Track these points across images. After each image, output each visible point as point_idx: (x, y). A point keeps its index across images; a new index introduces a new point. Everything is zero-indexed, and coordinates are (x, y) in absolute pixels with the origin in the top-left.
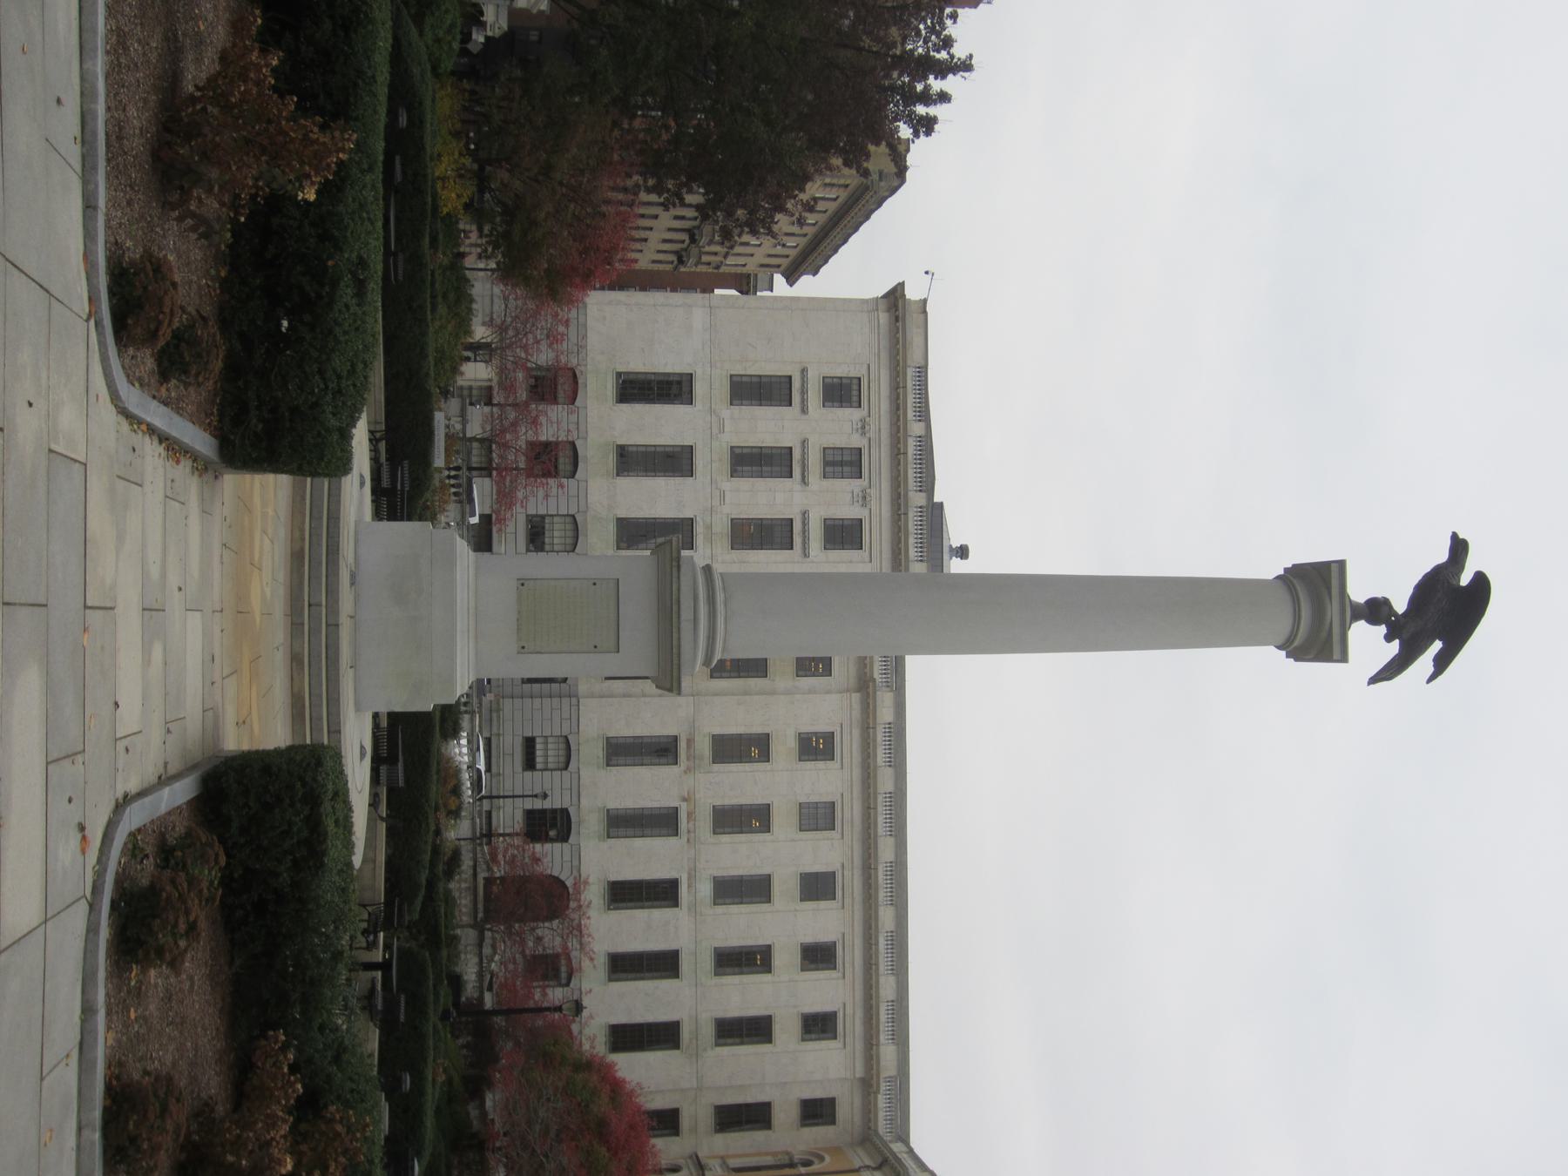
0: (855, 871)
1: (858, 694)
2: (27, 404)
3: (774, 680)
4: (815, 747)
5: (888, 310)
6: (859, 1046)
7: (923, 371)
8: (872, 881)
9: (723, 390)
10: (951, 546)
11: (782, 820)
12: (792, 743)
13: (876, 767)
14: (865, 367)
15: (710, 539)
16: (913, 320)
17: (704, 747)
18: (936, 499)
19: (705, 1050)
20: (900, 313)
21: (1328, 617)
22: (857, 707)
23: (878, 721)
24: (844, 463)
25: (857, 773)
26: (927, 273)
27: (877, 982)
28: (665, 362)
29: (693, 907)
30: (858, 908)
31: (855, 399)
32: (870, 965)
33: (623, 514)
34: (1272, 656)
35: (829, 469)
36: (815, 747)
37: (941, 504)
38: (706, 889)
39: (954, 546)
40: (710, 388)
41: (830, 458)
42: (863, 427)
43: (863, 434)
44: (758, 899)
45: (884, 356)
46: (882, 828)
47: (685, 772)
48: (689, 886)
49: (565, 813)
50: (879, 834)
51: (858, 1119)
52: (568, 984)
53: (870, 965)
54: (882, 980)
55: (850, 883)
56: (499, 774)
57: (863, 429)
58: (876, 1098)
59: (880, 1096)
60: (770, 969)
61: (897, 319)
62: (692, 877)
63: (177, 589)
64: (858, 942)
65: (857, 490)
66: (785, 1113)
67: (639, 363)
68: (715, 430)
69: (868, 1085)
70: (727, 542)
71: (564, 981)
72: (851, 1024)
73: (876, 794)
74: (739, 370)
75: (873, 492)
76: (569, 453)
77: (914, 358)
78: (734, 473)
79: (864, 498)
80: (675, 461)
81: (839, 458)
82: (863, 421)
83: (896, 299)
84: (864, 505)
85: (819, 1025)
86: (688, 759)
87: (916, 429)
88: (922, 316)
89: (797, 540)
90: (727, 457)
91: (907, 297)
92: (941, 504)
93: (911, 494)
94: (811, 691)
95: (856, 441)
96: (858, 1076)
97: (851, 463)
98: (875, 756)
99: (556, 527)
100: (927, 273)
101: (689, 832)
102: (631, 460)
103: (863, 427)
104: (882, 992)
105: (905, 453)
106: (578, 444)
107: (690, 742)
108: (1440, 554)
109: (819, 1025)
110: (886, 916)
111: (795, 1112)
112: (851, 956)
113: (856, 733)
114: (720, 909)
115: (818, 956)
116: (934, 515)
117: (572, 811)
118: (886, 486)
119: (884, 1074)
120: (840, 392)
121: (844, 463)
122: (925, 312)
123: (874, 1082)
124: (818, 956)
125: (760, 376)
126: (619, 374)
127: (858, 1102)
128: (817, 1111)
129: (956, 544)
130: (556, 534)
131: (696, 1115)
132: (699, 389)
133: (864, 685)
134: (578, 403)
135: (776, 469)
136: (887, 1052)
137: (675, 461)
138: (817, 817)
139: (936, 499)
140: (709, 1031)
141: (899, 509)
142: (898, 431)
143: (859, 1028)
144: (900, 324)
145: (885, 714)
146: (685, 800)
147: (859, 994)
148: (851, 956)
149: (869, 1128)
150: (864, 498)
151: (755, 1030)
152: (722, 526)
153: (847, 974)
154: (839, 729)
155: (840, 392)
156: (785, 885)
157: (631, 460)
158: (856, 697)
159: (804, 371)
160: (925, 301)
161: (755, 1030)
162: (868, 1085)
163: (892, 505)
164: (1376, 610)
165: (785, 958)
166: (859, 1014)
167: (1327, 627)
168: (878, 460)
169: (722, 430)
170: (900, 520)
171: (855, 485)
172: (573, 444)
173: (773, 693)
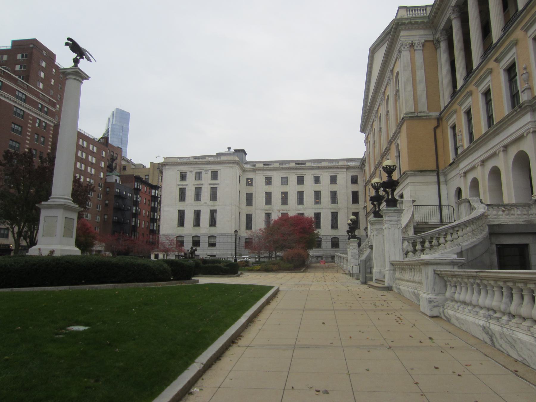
0: (297, 172)
1: (257, 172)
2: (368, 352)
3: (253, 191)
4: (268, 181)
5: (166, 166)
6: (338, 170)
7: (180, 158)
8: (299, 168)
9: (182, 203)
10: (228, 151)
11: (285, 189)
12: (267, 187)
13: (273, 167)
14: (178, 171)
15: (214, 206)
16: (168, 161)
17: (268, 207)
18: (216, 155)
19: (338, 206)
20: (166, 164)
21: (70, 72)
22: (259, 172)
23: (295, 166)
24: (199, 176)
25: (274, 172)
26: (157, 158)
27: (324, 166)
28: (176, 216)
29: (305, 209)
30: (305, 171)
31: (185, 173)
32: (319, 168)
33: (209, 225)
34: (82, 85)
35: (200, 179)
36: (268, 181)
37: (217, 154)
38: (300, 206)
39: (228, 150)
40: (181, 206)
41: (198, 179)
42: (191, 171)
43: (192, 171)
44: (320, 194)
45: (175, 167)
46: (271, 166)
47: (273, 211)
48: (299, 210)
49: (332, 239)
50: (289, 166)
51: (356, 170)
52: (322, 238)
53: (319, 168)
54: (323, 165)
55: (300, 173)
56: (323, 254)
57: (191, 171)
58: (351, 166)
59: (350, 165)
60: (286, 192)
61: (167, 164)
62: (297, 210)
63: (323, 322)
64: (314, 171)
65: (205, 173)
66: (355, 187)
67: (176, 222)
68: (191, 205)
69: (348, 168)
70: (215, 202)
71: (321, 239)
72: (333, 172)
73: (279, 167)
74: (178, 200)
75: (205, 169)
76: (179, 238)
77: (176, 160)
78: (200, 201)
79: (206, 171)
80: (197, 214)
81: (198, 177)
82: (190, 171)
83: (163, 164)
84: (208, 171)
85: (333, 179)
86: (270, 211)
87: (192, 160)
88: (167, 158)
89: (215, 186)
90: (197, 202)
91: (163, 162)
92: (217, 154)
93: (206, 160)
94: (256, 183)
95: (194, 173)
96: (345, 170)
97: (199, 174)
98: (270, 168)
99: (211, 241)
100: (157, 158)
101: (287, 210)
102: (197, 223)
103: (191, 171)
104: (326, 165)
105: (196, 162)
106: (193, 236)
107: (266, 210)
108: (68, 47)
109: (333, 179)
110: (308, 164)
111: (354, 185)
112: (317, 172)
113: (265, 172)
114: (305, 203)
115: (317, 180)
116: (219, 155)
117: (332, 237)
118: (204, 166)
119: (346, 164)
120: (183, 177)
121: (199, 176)
122: (166, 158)
123: (347, 167)
124: (317, 180)
125: (195, 195)
126: (178, 226)
127: (352, 170)
128: (354, 180)
129: (227, 150)
130: (212, 241)
131: (354, 208)
132: (181, 209)
133: (254, 170)
134: (184, 236)
135: (200, 191)
136: (340, 164)
137: (197, 214)
138: (284, 180)
139: (216, 155)
140: (334, 206)
141: (209, 163)
142: (191, 163)
143: (334, 170)
144: (168, 163)
145: (261, 165)
146: (279, 211)
147: (326, 170)
148: (317, 172)
149: (359, 167)
150: (206, 171)
151: (334, 195)
152: (212, 203)
153: (321, 173)
154: (264, 176)
155: (183, 177)
156: (300, 188)
157: (197, 223)
158: (257, 172)
159: (179, 185)
160: (164, 158)
161: (334, 195)
162: (348, 168)
163: (208, 164)
164: (76, 61)
165: (317, 188)
166: (331, 170)
167: (72, 72)
168: (198, 168)
169: (191, 203)
170: (211, 163)
171: (203, 173)
172: (193, 237)
173: (256, 191)
